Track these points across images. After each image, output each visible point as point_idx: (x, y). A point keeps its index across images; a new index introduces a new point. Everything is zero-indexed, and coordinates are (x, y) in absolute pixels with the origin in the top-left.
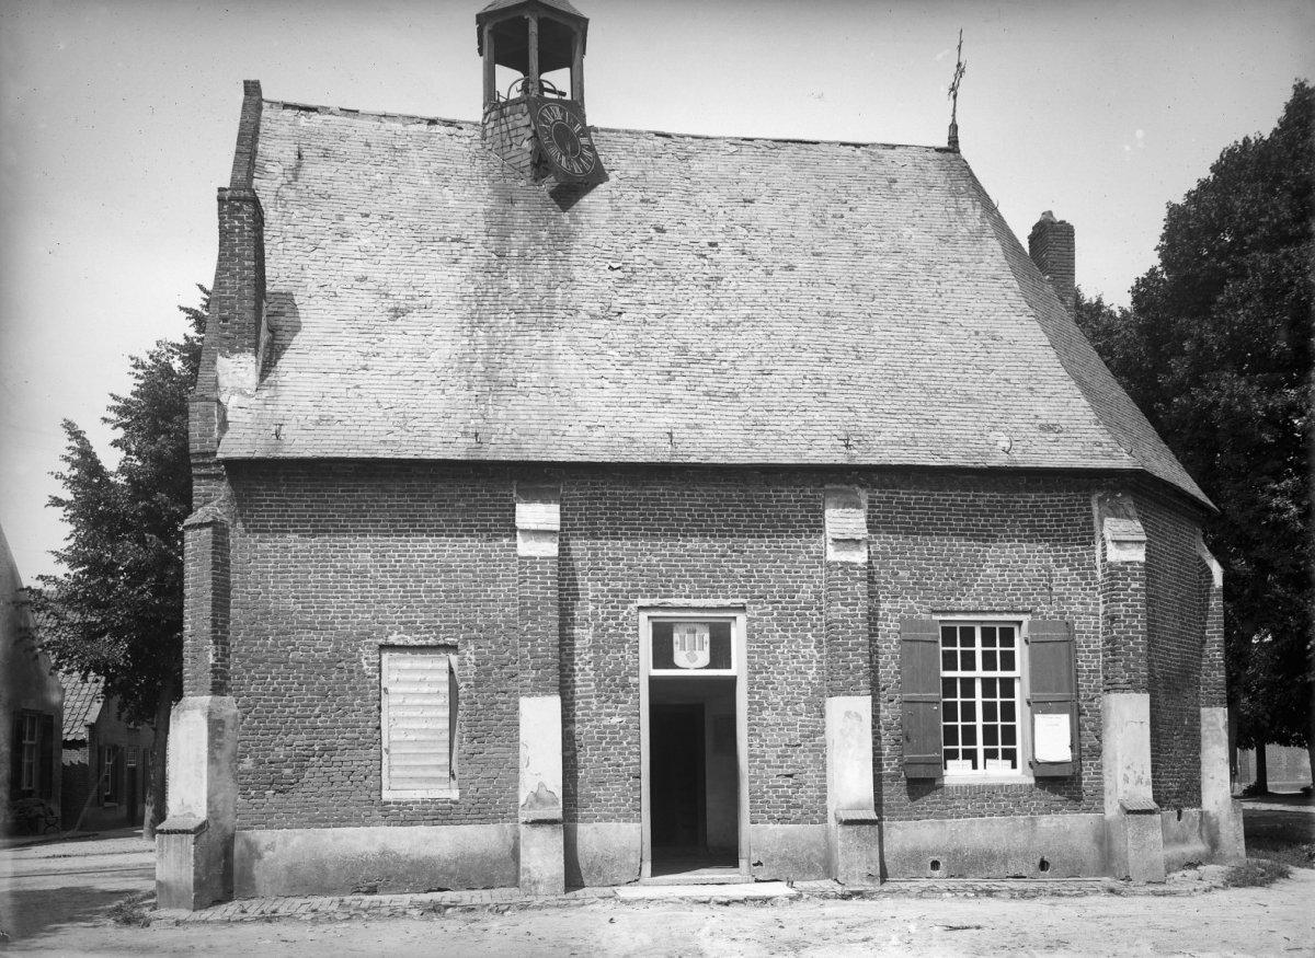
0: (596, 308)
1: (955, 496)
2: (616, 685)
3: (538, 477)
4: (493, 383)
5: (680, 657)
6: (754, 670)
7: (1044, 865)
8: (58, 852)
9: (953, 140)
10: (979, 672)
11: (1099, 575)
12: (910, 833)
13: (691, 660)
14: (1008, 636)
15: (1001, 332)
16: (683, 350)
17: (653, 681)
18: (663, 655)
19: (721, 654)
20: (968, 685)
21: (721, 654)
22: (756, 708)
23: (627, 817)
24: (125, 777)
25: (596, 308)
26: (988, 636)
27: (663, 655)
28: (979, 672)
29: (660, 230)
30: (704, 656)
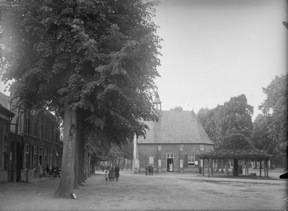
0: (163, 130)
1: (190, 145)
2: (165, 159)
3: (159, 144)
4: (156, 137)
5: (169, 157)
6: (174, 158)
7: (196, 172)
8: (184, 178)
9: (193, 110)
10: (191, 158)
11: (250, 131)
12: (186, 170)
13: (170, 157)
14: (193, 155)
15: (195, 131)
16: (170, 133)
17: (167, 158)
18: (168, 157)
19: (172, 157)
20: (190, 159)
21: (172, 157)
22: (175, 160)
23: (166, 168)
24: (49, 117)
25: (163, 130)
26: (192, 155)
27: (168, 157)
28: (191, 158)
29: (168, 121)
30: (171, 157)
